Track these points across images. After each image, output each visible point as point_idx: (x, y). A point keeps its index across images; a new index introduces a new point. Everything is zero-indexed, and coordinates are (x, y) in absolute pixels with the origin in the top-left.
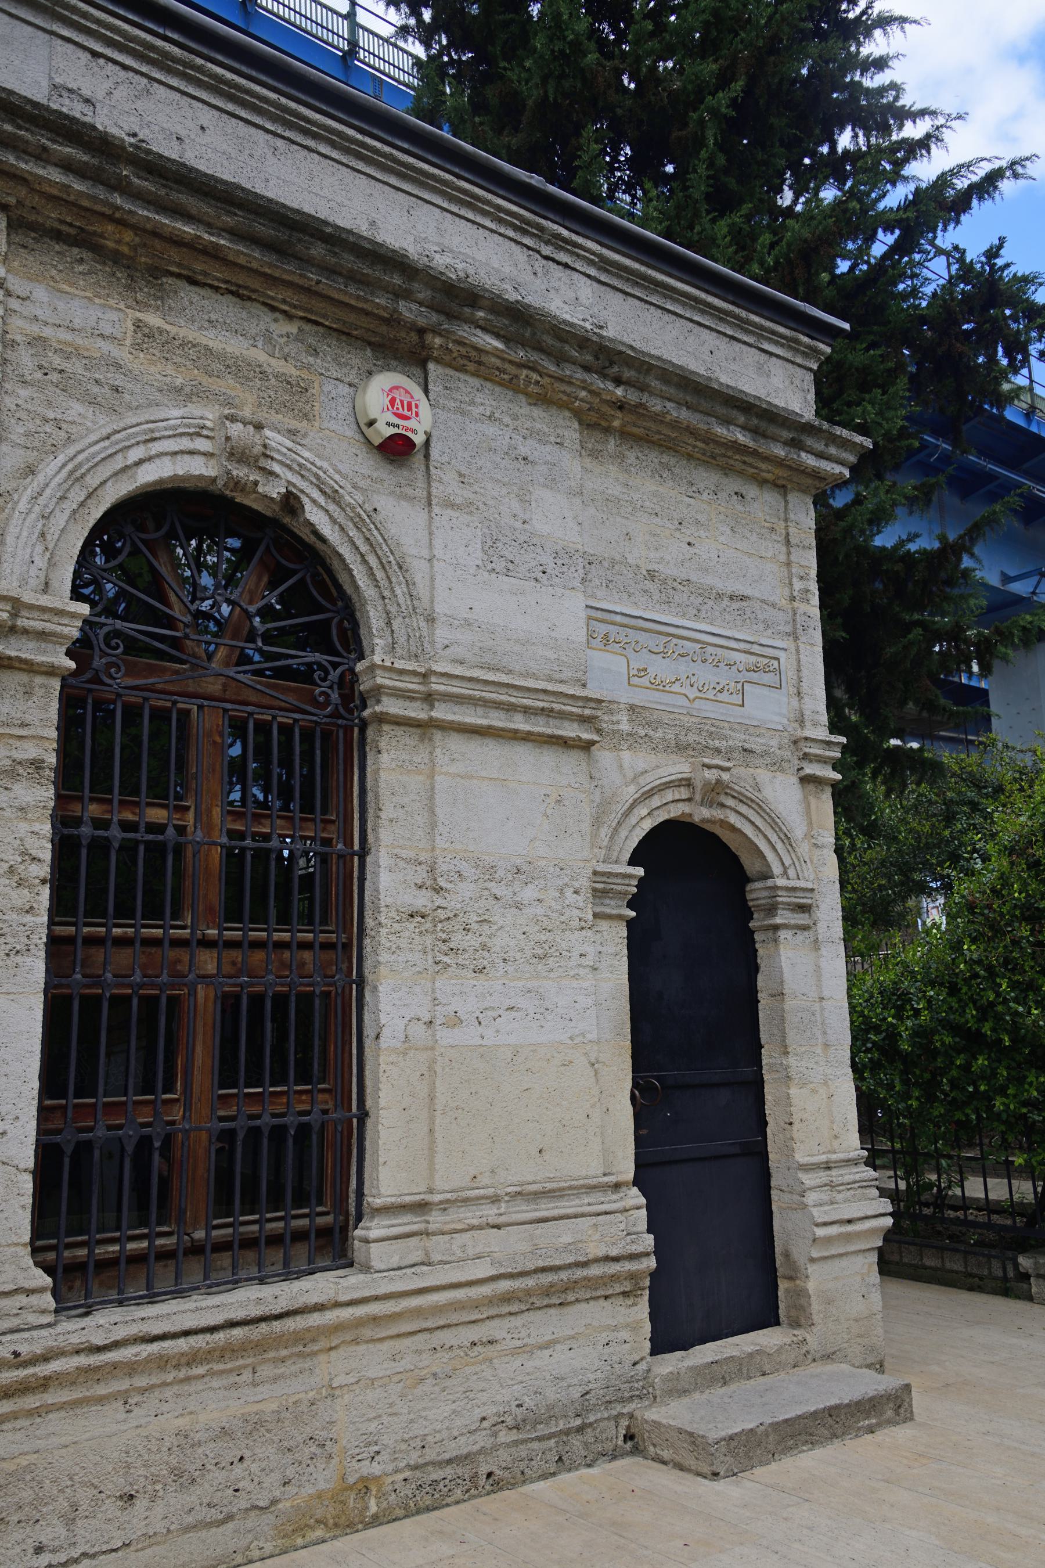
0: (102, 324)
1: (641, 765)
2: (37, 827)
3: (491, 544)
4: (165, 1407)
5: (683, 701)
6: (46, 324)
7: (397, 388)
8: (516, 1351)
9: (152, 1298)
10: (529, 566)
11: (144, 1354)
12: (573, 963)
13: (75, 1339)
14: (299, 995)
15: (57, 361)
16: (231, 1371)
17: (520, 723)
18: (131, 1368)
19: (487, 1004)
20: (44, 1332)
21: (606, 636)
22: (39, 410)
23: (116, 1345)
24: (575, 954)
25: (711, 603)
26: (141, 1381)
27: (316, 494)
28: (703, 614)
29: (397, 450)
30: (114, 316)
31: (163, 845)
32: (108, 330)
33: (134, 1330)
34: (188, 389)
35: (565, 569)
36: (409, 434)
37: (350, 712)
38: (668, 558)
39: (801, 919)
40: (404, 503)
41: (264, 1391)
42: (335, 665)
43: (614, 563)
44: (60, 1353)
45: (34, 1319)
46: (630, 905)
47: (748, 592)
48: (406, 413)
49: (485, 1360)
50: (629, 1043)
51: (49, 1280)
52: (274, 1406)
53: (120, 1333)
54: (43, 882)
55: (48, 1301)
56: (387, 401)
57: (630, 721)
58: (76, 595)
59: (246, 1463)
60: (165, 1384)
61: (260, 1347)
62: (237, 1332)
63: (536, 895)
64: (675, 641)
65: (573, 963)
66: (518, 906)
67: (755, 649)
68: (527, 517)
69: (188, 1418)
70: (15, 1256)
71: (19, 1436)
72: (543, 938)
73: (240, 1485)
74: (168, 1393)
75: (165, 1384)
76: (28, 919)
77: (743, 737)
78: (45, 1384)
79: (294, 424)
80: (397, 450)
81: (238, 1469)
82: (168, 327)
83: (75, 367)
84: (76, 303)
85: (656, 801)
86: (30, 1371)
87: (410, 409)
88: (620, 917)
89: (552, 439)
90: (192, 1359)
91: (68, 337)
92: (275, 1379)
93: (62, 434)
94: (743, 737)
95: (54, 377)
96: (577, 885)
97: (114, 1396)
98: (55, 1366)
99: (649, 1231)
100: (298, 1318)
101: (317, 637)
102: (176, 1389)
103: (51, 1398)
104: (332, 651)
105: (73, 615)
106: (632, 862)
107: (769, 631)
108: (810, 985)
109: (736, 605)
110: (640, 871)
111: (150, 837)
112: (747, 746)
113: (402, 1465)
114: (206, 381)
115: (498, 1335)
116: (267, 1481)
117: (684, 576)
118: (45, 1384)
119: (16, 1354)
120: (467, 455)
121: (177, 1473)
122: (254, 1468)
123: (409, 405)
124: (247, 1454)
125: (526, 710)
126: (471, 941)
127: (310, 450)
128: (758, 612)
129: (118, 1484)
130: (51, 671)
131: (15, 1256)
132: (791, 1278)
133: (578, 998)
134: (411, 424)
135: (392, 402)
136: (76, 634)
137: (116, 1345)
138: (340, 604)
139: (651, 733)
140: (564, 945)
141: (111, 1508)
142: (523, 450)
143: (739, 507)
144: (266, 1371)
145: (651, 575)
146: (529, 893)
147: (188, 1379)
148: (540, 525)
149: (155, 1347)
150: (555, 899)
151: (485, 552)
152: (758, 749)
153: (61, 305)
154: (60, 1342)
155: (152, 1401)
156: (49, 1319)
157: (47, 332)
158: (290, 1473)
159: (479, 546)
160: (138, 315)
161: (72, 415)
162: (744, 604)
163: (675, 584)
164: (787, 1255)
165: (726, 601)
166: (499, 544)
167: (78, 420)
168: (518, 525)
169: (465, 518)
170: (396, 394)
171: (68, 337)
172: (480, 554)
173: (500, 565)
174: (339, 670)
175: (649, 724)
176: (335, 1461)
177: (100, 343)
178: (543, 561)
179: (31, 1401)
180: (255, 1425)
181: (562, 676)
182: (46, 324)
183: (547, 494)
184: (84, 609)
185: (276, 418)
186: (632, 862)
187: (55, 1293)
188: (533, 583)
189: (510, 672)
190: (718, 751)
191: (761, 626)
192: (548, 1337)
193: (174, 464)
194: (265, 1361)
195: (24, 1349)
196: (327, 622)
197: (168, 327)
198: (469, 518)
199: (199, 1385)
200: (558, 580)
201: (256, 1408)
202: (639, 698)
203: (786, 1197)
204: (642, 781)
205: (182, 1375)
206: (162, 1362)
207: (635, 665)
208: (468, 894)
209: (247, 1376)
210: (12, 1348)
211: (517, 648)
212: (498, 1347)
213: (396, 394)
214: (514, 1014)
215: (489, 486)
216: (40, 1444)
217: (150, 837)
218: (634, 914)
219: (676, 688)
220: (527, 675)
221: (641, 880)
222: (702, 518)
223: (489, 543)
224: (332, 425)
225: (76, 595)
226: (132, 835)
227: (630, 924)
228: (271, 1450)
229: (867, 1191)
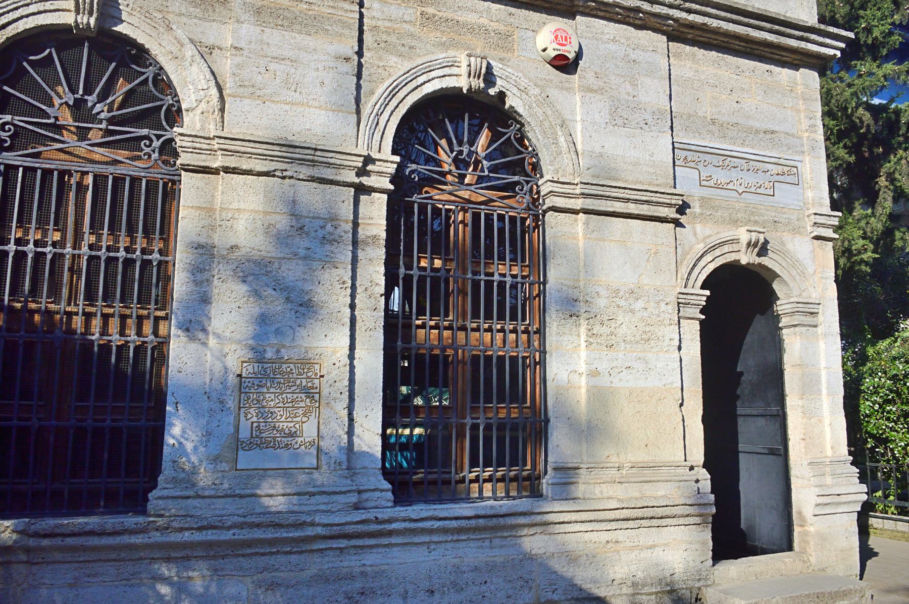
0: (405, 16)
1: (708, 232)
2: (378, 269)
3: (614, 111)
4: (447, 553)
5: (735, 194)
6: (379, 19)
7: (558, 29)
8: (632, 549)
9: (441, 501)
10: (637, 121)
11: (436, 526)
12: (665, 344)
13: (403, 515)
14: (511, 357)
15: (384, 37)
16: (479, 539)
17: (632, 208)
18: (431, 531)
19: (614, 365)
20: (389, 510)
21: (686, 158)
22: (376, 62)
23: (422, 520)
24: (667, 339)
25: (751, 136)
26: (435, 538)
27: (515, 90)
28: (747, 143)
29: (565, 65)
30: (411, 11)
31: (439, 277)
32: (406, 18)
33: (430, 514)
34: (447, 44)
35: (659, 121)
36: (566, 54)
37: (537, 207)
38: (723, 111)
39: (809, 320)
40: (564, 92)
41: (496, 552)
42: (528, 182)
43: (690, 116)
44: (395, 520)
45: (384, 503)
46: (701, 312)
47: (777, 129)
48: (564, 42)
49: (615, 551)
50: (701, 389)
51: (390, 486)
52: (502, 560)
53: (424, 514)
54: (382, 295)
55: (390, 495)
56: (553, 37)
57: (701, 206)
58: (394, 152)
59: (488, 584)
60: (447, 541)
61: (494, 529)
62: (481, 521)
63: (643, 306)
64: (729, 159)
65: (665, 344)
66: (633, 311)
67: (782, 161)
68: (636, 94)
69: (458, 560)
70: (374, 473)
71: (379, 556)
72: (648, 329)
73: (486, 594)
74: (449, 546)
75: (447, 541)
76: (375, 313)
77: (774, 214)
78: (390, 533)
79: (504, 55)
80: (565, 65)
81: (484, 588)
82: (438, 13)
83: (393, 39)
84: (393, 7)
85: (718, 252)
86: (382, 527)
87: (566, 40)
88: (697, 319)
89: (651, 49)
90: (460, 531)
91: (387, 24)
92: (501, 547)
93: (387, 73)
94: (774, 214)
95: (382, 45)
96: (668, 300)
97: (423, 543)
98: (395, 526)
99: (712, 493)
100: (512, 518)
101: (517, 167)
102: (452, 544)
103: (394, 540)
104: (527, 175)
105: (392, 162)
106: (702, 288)
107: (790, 151)
108: (813, 355)
109: (768, 136)
110: (708, 293)
111: (432, 274)
112: (776, 219)
113: (570, 597)
114: (456, 37)
115: (621, 539)
116: (499, 595)
117: (734, 121)
118: (390, 533)
119: (377, 518)
120: (600, 63)
121: (454, 584)
122: (492, 587)
123: (566, 38)
124: (489, 581)
125: (636, 201)
126: (605, 330)
127: (512, 68)
128: (783, 140)
129: (426, 584)
130: (382, 191)
131: (374, 473)
132: (801, 526)
133: (669, 363)
134: (567, 48)
135: (556, 37)
136: (393, 171)
137: (422, 520)
138: (530, 149)
139: (714, 213)
140: (660, 334)
141: (422, 595)
142: (633, 57)
143: (769, 79)
144: (497, 542)
145: (713, 122)
146: (639, 304)
147: (458, 541)
148: (643, 97)
149: (441, 523)
150: (654, 308)
151: (611, 115)
152: (783, 221)
153: (386, 9)
154: (395, 515)
155: (441, 549)
156: (390, 504)
157: (379, 23)
158: (510, 592)
159: (607, 112)
160: (423, 9)
161: (391, 63)
162: (773, 135)
163: (729, 126)
164: (800, 513)
165: (762, 135)
166: (619, 110)
167: (394, 65)
168: (631, 98)
169: (598, 97)
170: (558, 33)
171: (387, 24)
172: (608, 116)
173: (620, 122)
174: (530, 185)
175: (713, 207)
176: (534, 590)
177: (405, 25)
178: (647, 117)
179: (385, 541)
180: (491, 568)
181: (658, 182)
182: (379, 19)
183: (648, 81)
184: (397, 159)
185: (493, 53)
186: (702, 288)
187: (393, 492)
188: (640, 130)
189: (626, 181)
190: (756, 222)
191: (785, 149)
192: (651, 543)
193: (441, 82)
194: (495, 537)
195: (380, 516)
196: (524, 158)
197: (438, 13)
198: (601, 97)
199: (464, 544)
200: (654, 128)
201: (492, 559)
202: (705, 192)
203: (800, 481)
204: (708, 241)
205: (455, 538)
206: (445, 531)
207: (704, 175)
208: (603, 305)
209: (487, 543)
210: (375, 515)
211: (630, 168)
212: (622, 545)
213: (558, 33)
214: (630, 371)
215: (613, 78)
216: (390, 561)
217: (432, 274)
218: (704, 317)
219: (730, 186)
220: (636, 183)
221: (708, 297)
222: (746, 87)
223: (613, 109)
224: (524, 53)
225: (394, 152)
226: (423, 273)
227: (702, 323)
228: (501, 580)
229: (851, 479)
